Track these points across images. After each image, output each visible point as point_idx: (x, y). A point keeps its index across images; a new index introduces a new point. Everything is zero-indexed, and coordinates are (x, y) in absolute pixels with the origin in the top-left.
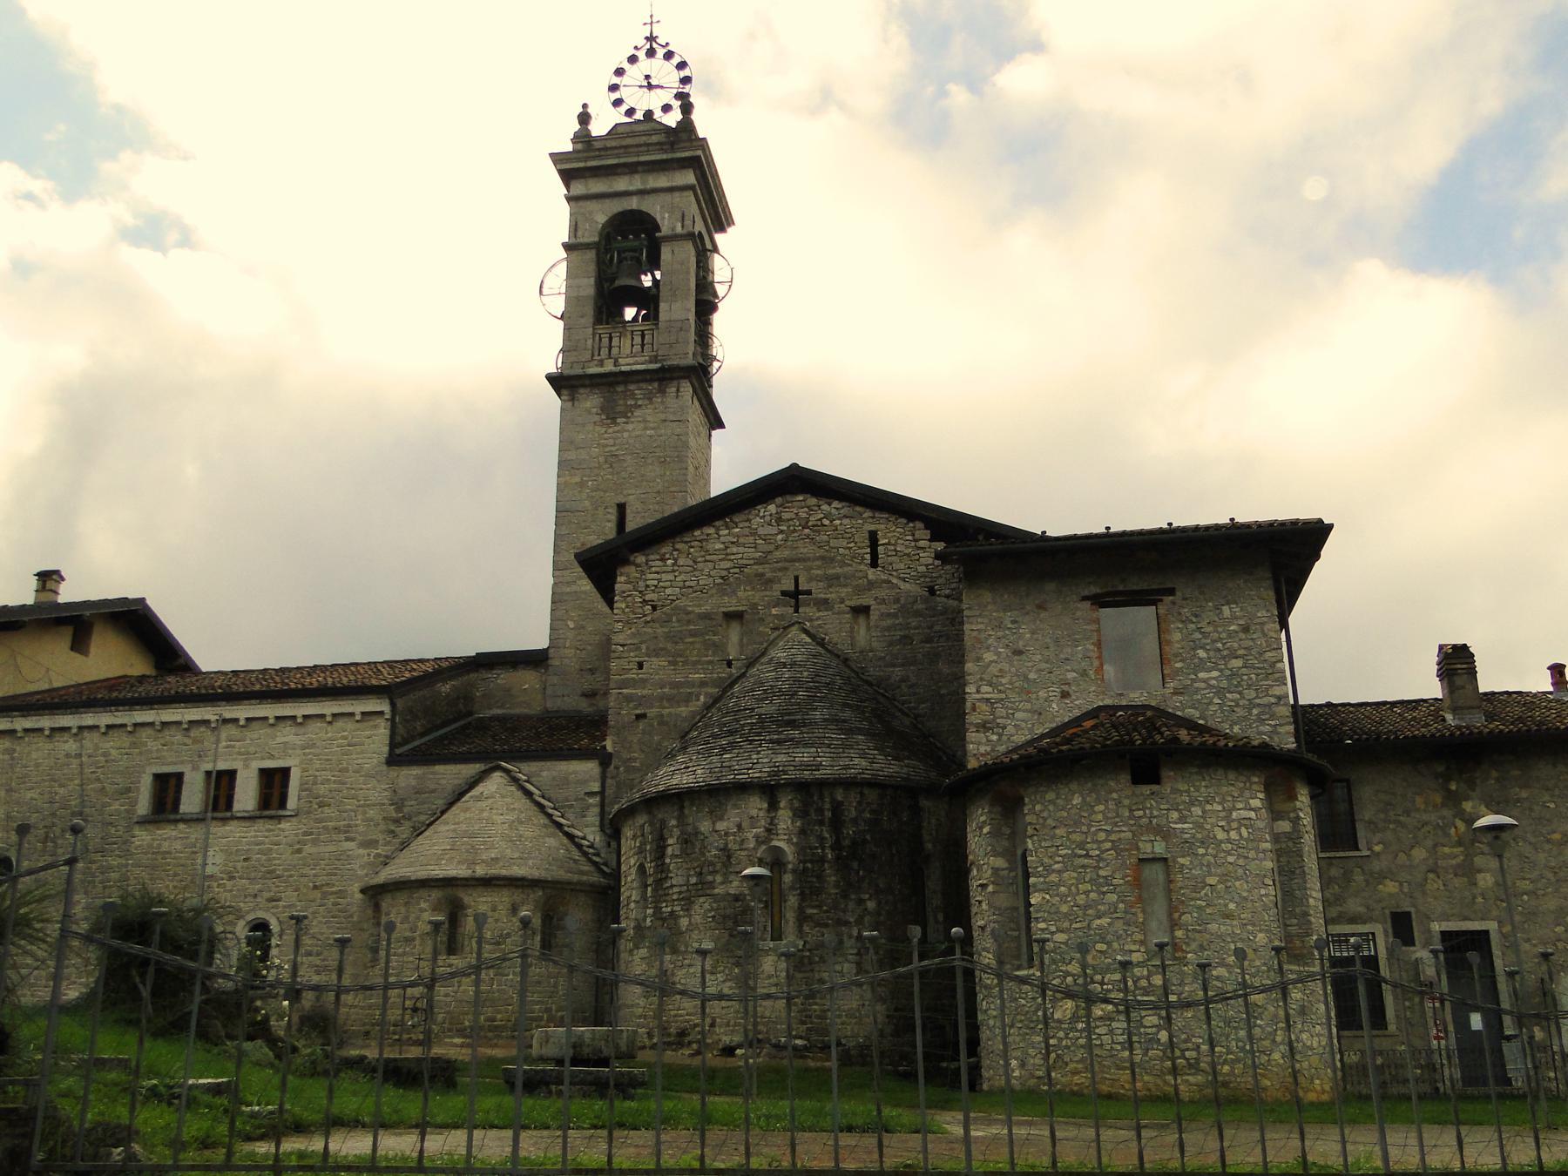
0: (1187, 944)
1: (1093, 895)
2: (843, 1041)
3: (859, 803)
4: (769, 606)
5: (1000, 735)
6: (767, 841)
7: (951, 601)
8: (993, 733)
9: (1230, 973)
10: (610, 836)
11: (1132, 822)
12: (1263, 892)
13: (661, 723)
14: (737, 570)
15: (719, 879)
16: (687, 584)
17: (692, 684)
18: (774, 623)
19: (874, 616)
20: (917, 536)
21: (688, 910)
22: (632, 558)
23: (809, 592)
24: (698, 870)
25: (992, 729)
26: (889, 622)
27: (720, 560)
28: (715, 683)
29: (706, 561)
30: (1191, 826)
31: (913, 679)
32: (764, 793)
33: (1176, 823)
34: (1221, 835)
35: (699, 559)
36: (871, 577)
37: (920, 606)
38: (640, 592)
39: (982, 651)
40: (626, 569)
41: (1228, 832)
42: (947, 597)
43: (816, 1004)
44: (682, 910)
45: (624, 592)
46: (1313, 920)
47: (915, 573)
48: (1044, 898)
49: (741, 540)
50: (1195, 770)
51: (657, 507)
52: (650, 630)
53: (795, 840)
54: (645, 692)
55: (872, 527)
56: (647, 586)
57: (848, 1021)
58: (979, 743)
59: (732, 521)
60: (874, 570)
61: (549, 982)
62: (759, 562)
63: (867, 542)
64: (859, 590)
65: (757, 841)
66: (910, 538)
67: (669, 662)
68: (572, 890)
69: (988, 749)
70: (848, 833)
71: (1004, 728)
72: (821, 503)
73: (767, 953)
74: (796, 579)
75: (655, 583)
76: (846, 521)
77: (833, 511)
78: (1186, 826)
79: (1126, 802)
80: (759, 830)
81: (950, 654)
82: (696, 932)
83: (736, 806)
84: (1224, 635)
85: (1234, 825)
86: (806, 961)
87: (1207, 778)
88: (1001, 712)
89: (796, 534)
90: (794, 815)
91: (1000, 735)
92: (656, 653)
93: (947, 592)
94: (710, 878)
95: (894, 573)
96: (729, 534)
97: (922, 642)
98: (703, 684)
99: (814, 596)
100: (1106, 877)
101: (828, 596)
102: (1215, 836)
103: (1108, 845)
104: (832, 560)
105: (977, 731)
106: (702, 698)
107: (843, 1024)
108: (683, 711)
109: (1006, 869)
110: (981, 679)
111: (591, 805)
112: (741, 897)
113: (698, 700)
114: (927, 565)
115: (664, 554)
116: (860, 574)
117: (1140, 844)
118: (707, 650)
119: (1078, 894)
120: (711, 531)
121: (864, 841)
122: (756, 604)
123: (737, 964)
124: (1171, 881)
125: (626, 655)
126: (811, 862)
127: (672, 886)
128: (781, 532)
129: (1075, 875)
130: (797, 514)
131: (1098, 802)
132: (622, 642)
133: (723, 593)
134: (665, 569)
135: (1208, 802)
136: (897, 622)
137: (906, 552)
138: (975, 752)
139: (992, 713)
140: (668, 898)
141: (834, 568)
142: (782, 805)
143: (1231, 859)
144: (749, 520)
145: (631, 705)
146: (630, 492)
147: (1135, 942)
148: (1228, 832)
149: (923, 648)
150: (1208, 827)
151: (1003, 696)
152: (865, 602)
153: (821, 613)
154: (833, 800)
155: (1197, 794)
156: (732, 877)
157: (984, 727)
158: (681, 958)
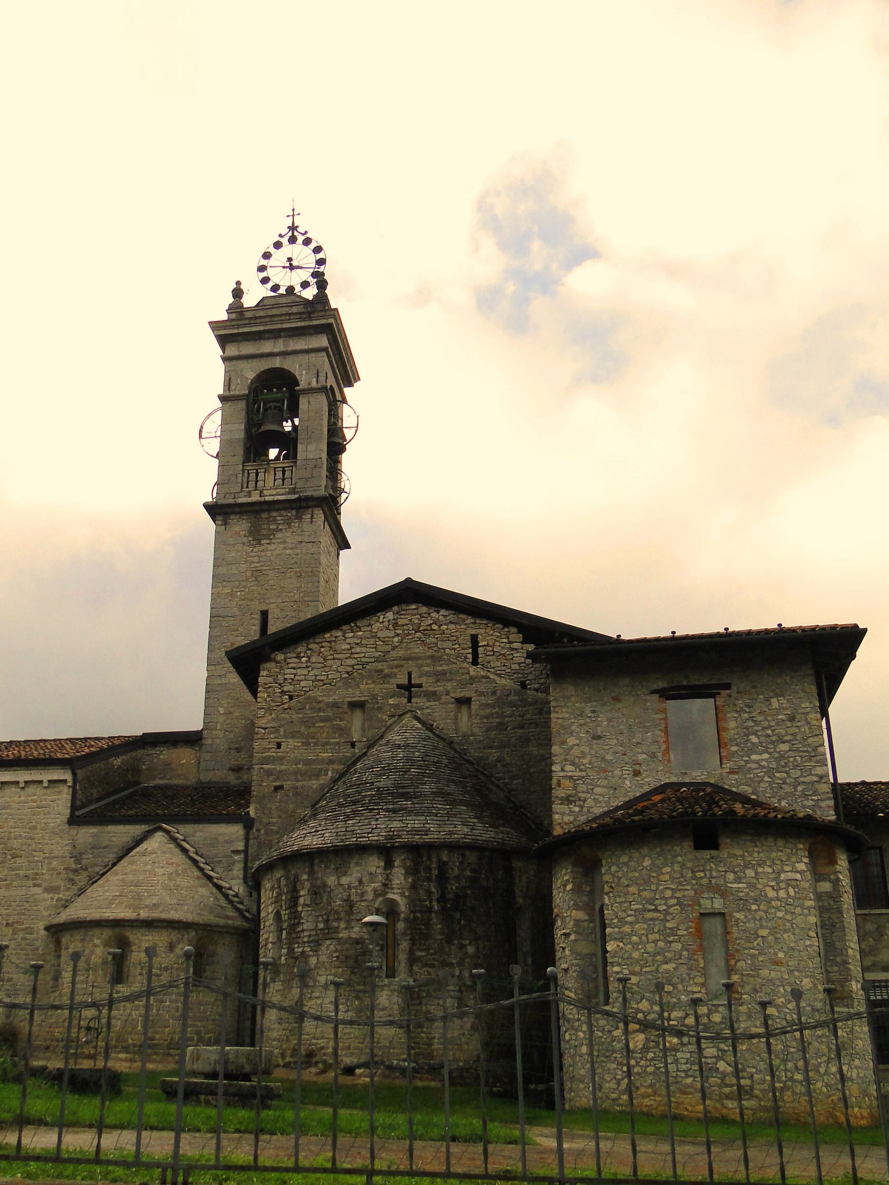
0: (742, 987)
1: (661, 944)
3: (461, 863)
4: (385, 697)
5: (581, 807)
6: (384, 893)
8: (575, 806)
9: (779, 1012)
11: (694, 882)
12: (808, 943)
13: (296, 794)
15: (342, 925)
16: (318, 678)
17: (322, 761)
19: (474, 706)
20: (510, 639)
22: (272, 656)
23: (420, 686)
26: (488, 711)
27: (346, 658)
28: (341, 761)
29: (334, 659)
30: (745, 885)
31: (507, 760)
32: (381, 853)
33: (733, 883)
34: (771, 894)
36: (472, 673)
37: (513, 698)
38: (280, 684)
40: (268, 665)
41: (777, 891)
43: (423, 1032)
45: (266, 684)
46: (851, 967)
48: (618, 946)
49: (364, 642)
50: (749, 838)
53: (407, 894)
54: (283, 767)
55: (474, 632)
56: (285, 679)
59: (356, 625)
60: (474, 667)
64: (463, 684)
67: (302, 743)
68: (220, 932)
69: (571, 818)
70: (452, 889)
71: (585, 801)
74: (410, 674)
75: (292, 676)
76: (452, 626)
77: (441, 617)
78: (741, 885)
79: (690, 865)
80: (377, 885)
83: (357, 864)
84: (772, 724)
85: (783, 885)
87: (759, 845)
88: (582, 787)
90: (406, 873)
91: (581, 807)
93: (536, 686)
94: (335, 924)
95: (492, 670)
96: (353, 637)
97: (514, 729)
98: (331, 761)
99: (424, 688)
100: (671, 929)
101: (436, 689)
102: (766, 894)
103: (674, 901)
104: (440, 658)
106: (330, 773)
108: (315, 784)
109: (586, 920)
110: (566, 760)
113: (326, 775)
114: (519, 664)
115: (300, 653)
116: (464, 671)
117: (702, 901)
119: (648, 942)
120: (339, 634)
122: (375, 695)
123: (358, 998)
124: (728, 933)
126: (420, 912)
128: (398, 635)
129: (646, 926)
130: (410, 620)
131: (665, 864)
132: (264, 726)
133: (347, 686)
135: (760, 865)
136: (494, 711)
137: (502, 652)
138: (560, 821)
139: (575, 788)
141: (441, 665)
142: (396, 864)
143: (780, 914)
144: (370, 625)
145: (271, 778)
147: (696, 984)
148: (777, 891)
150: (760, 887)
151: (584, 774)
152: (467, 695)
153: (429, 703)
155: (749, 858)
157: (568, 800)
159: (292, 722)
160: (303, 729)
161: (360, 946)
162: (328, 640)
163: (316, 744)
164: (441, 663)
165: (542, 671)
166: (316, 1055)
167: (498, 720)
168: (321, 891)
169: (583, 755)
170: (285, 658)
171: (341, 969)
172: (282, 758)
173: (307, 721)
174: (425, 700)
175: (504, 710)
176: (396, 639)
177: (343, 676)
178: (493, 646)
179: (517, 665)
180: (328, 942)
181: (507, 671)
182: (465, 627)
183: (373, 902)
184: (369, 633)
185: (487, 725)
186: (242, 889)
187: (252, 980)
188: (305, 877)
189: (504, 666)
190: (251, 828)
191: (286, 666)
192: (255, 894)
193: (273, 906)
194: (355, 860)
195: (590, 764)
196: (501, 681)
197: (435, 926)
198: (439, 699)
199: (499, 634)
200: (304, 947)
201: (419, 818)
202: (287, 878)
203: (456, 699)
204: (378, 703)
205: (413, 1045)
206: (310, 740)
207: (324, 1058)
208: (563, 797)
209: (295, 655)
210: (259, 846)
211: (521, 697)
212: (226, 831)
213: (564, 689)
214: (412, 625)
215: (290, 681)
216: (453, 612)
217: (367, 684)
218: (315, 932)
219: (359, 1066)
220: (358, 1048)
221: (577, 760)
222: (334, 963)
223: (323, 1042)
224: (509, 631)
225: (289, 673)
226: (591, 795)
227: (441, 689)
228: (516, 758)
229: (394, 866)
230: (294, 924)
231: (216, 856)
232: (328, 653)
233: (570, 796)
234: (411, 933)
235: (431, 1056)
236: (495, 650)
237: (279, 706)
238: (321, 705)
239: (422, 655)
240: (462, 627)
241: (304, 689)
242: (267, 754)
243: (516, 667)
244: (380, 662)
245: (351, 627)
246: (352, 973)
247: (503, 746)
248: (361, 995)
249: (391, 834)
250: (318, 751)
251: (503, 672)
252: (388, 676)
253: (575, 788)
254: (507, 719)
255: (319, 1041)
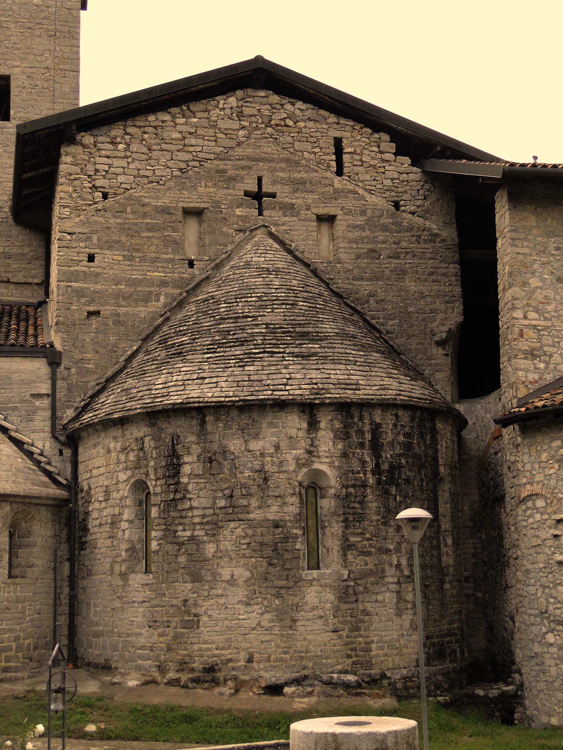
2: (388, 674)
3: (395, 425)
4: (231, 206)
5: (547, 363)
6: (308, 463)
7: (417, 218)
8: (540, 361)
10: (63, 444)
13: (118, 323)
14: (197, 164)
15: (254, 503)
16: (142, 173)
17: (151, 283)
18: (237, 224)
19: (340, 226)
20: (382, 148)
21: (214, 535)
22: (78, 137)
23: (273, 195)
24: (227, 492)
25: (539, 356)
26: (357, 234)
27: (178, 151)
28: (176, 284)
29: (162, 150)
31: (381, 295)
32: (303, 411)
35: (155, 147)
36: (337, 185)
37: (386, 220)
38: (89, 176)
39: (528, 275)
40: (72, 149)
42: (413, 213)
43: (361, 636)
44: (207, 534)
45: (71, 175)
47: (380, 186)
49: (200, 132)
51: (46, 85)
52: (101, 219)
53: (337, 464)
54: (98, 287)
55: (338, 134)
56: (97, 170)
57: (389, 652)
58: (528, 371)
59: (189, 109)
60: (339, 178)
61: (17, 608)
62: (218, 157)
63: (333, 149)
64: (326, 199)
65: (297, 464)
66: (376, 149)
67: (124, 256)
68: (36, 504)
69: (537, 377)
70: (386, 457)
71: (551, 356)
72: (283, 101)
73: (311, 582)
74: (260, 179)
75: (106, 168)
76: (311, 124)
77: (297, 112)
80: (299, 452)
81: (417, 272)
82: (226, 560)
83: (271, 425)
86: (351, 591)
88: (547, 340)
89: (259, 132)
90: (335, 437)
91: (547, 363)
92: (111, 245)
93: (413, 208)
94: (244, 502)
95: (361, 184)
96: (186, 124)
97: (389, 257)
98: (163, 283)
104: (298, 163)
105: (526, 358)
106: (162, 299)
107: (385, 656)
108: (142, 311)
110: (528, 305)
111: (38, 408)
112: (281, 523)
113: (158, 300)
114: (392, 179)
115: (116, 137)
116: (327, 182)
118: (167, 247)
120: (167, 117)
121: (400, 466)
122: (218, 202)
123: (278, 596)
125: (74, 244)
126: (354, 486)
127: (191, 508)
128: (243, 128)
130: (259, 110)
132: (69, 230)
133: (183, 187)
134: (116, 153)
136: (364, 234)
137: (372, 163)
138: (524, 379)
139: (539, 339)
140: (186, 521)
141: (299, 172)
142: (322, 425)
144: (206, 111)
145: (83, 300)
146: (15, 63)
149: (390, 263)
151: (549, 324)
152: (332, 211)
153: (286, 219)
154: (372, 422)
156: (270, 502)
157: (532, 354)
158: (207, 587)
159: (108, 228)
160: (124, 239)
161: (280, 530)
162: (152, 124)
163: (142, 259)
164: (298, 169)
165: (418, 191)
166: (220, 670)
167: (369, 246)
168: (220, 458)
169: (547, 301)
170: (95, 142)
171: (253, 560)
172: (98, 275)
173: (129, 229)
174: (280, 213)
175: (376, 234)
176: (242, 133)
177: (175, 173)
178: (361, 154)
179: (389, 181)
180: (232, 525)
181: (378, 186)
182: (325, 126)
183: (294, 474)
184: (206, 121)
185: (357, 251)
186: (48, 445)
187: (67, 564)
188: (192, 438)
189: (374, 180)
190: (58, 364)
191: (97, 154)
192: (67, 452)
193: (129, 473)
194: (268, 420)
195: (556, 311)
196: (372, 199)
197: (370, 504)
198: (298, 215)
199: (367, 140)
200: (194, 530)
201: (338, 367)
202: (157, 438)
203: (317, 216)
204: (221, 212)
205: (349, 652)
206: (134, 254)
207: (234, 673)
208: (525, 350)
209: (108, 140)
210: (69, 390)
211: (395, 220)
212: (21, 367)
213: (523, 218)
214: (261, 117)
215: (104, 173)
216: (312, 106)
217: (206, 186)
218: (211, 511)
219: (287, 684)
220: (281, 660)
221: (540, 306)
222: (242, 552)
223: (230, 654)
224: (380, 139)
225: (102, 163)
226: (558, 350)
227: (299, 201)
228: (391, 294)
229: (320, 428)
230: (174, 500)
231: (10, 401)
232: (152, 141)
233: (534, 349)
234: (344, 514)
235: (369, 665)
236: (364, 159)
237: (90, 205)
238: (147, 209)
239: (275, 156)
240: (324, 126)
241: (123, 186)
242: (76, 268)
243: (388, 182)
244: (223, 160)
245: (182, 110)
246: (270, 564)
247: (376, 278)
248: (283, 591)
249: (316, 387)
250: (146, 268)
251: (374, 188)
252: (232, 179)
253: (539, 339)
254: (380, 246)
255: (223, 652)
